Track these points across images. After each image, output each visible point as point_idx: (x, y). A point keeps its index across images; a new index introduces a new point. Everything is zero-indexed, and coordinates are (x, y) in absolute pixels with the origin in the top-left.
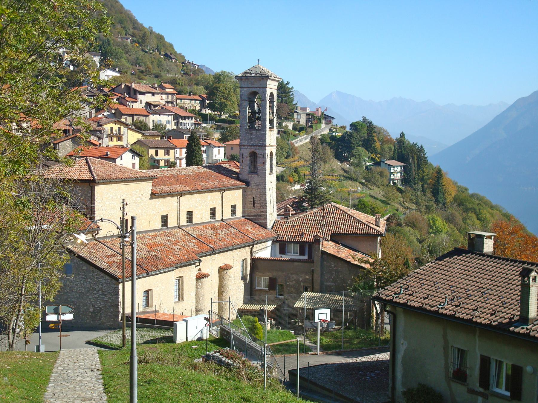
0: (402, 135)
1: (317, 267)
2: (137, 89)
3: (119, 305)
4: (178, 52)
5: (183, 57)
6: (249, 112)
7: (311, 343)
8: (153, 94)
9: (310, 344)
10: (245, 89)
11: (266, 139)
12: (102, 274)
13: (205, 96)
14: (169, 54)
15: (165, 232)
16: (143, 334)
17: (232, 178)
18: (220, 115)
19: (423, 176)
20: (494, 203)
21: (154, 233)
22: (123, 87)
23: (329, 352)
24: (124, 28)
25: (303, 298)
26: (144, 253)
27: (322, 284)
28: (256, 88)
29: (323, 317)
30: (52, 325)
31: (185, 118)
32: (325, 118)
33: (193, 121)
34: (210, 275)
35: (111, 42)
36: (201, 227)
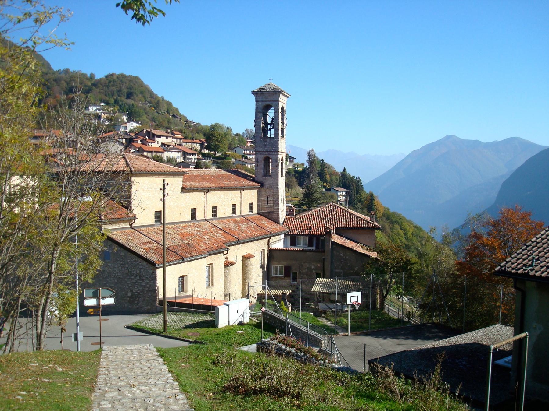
0: (345, 170)
1: (327, 256)
2: (155, 133)
3: (156, 290)
4: (182, 114)
5: (186, 117)
6: (263, 123)
7: (333, 324)
8: (167, 137)
9: (332, 325)
10: (260, 103)
11: (278, 145)
12: (140, 260)
13: (204, 140)
14: (175, 115)
15: (194, 224)
16: (181, 318)
17: (248, 180)
18: (215, 154)
19: (361, 199)
20: (407, 219)
21: (184, 225)
22: (144, 132)
23: (358, 333)
24: (144, 97)
25: (318, 283)
26: (177, 241)
27: (331, 271)
28: (270, 101)
29: (354, 300)
30: (91, 310)
31: (190, 154)
32: (289, 158)
33: (196, 157)
34: (235, 263)
35: (135, 106)
36: (225, 221)
